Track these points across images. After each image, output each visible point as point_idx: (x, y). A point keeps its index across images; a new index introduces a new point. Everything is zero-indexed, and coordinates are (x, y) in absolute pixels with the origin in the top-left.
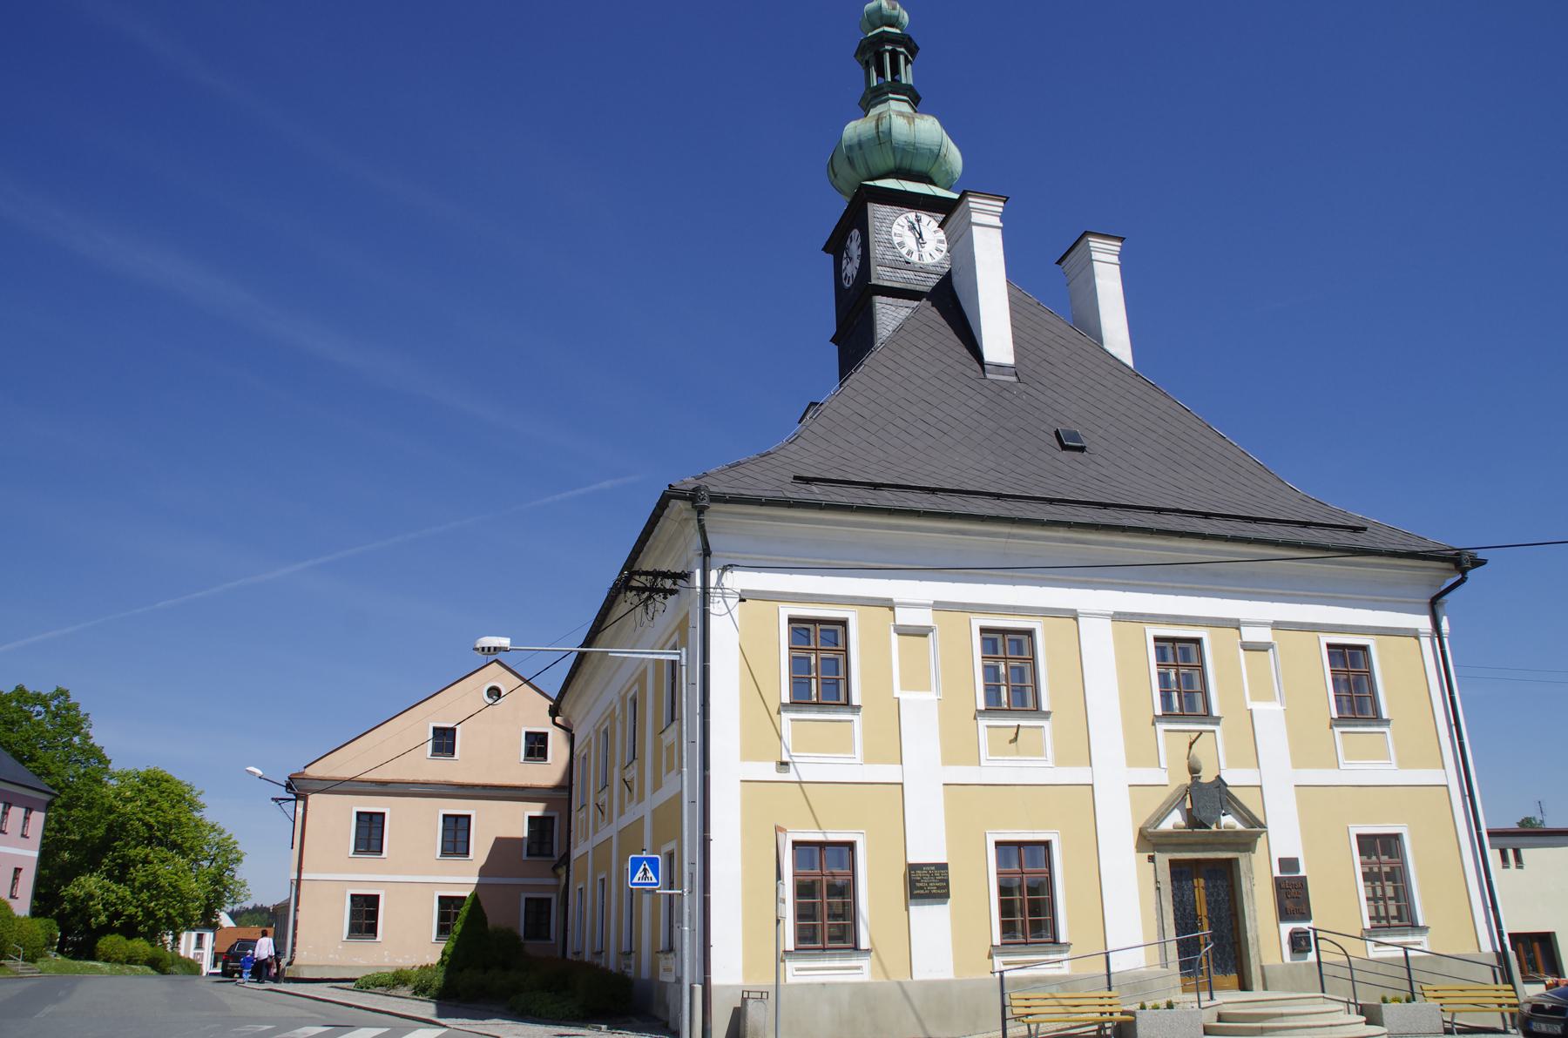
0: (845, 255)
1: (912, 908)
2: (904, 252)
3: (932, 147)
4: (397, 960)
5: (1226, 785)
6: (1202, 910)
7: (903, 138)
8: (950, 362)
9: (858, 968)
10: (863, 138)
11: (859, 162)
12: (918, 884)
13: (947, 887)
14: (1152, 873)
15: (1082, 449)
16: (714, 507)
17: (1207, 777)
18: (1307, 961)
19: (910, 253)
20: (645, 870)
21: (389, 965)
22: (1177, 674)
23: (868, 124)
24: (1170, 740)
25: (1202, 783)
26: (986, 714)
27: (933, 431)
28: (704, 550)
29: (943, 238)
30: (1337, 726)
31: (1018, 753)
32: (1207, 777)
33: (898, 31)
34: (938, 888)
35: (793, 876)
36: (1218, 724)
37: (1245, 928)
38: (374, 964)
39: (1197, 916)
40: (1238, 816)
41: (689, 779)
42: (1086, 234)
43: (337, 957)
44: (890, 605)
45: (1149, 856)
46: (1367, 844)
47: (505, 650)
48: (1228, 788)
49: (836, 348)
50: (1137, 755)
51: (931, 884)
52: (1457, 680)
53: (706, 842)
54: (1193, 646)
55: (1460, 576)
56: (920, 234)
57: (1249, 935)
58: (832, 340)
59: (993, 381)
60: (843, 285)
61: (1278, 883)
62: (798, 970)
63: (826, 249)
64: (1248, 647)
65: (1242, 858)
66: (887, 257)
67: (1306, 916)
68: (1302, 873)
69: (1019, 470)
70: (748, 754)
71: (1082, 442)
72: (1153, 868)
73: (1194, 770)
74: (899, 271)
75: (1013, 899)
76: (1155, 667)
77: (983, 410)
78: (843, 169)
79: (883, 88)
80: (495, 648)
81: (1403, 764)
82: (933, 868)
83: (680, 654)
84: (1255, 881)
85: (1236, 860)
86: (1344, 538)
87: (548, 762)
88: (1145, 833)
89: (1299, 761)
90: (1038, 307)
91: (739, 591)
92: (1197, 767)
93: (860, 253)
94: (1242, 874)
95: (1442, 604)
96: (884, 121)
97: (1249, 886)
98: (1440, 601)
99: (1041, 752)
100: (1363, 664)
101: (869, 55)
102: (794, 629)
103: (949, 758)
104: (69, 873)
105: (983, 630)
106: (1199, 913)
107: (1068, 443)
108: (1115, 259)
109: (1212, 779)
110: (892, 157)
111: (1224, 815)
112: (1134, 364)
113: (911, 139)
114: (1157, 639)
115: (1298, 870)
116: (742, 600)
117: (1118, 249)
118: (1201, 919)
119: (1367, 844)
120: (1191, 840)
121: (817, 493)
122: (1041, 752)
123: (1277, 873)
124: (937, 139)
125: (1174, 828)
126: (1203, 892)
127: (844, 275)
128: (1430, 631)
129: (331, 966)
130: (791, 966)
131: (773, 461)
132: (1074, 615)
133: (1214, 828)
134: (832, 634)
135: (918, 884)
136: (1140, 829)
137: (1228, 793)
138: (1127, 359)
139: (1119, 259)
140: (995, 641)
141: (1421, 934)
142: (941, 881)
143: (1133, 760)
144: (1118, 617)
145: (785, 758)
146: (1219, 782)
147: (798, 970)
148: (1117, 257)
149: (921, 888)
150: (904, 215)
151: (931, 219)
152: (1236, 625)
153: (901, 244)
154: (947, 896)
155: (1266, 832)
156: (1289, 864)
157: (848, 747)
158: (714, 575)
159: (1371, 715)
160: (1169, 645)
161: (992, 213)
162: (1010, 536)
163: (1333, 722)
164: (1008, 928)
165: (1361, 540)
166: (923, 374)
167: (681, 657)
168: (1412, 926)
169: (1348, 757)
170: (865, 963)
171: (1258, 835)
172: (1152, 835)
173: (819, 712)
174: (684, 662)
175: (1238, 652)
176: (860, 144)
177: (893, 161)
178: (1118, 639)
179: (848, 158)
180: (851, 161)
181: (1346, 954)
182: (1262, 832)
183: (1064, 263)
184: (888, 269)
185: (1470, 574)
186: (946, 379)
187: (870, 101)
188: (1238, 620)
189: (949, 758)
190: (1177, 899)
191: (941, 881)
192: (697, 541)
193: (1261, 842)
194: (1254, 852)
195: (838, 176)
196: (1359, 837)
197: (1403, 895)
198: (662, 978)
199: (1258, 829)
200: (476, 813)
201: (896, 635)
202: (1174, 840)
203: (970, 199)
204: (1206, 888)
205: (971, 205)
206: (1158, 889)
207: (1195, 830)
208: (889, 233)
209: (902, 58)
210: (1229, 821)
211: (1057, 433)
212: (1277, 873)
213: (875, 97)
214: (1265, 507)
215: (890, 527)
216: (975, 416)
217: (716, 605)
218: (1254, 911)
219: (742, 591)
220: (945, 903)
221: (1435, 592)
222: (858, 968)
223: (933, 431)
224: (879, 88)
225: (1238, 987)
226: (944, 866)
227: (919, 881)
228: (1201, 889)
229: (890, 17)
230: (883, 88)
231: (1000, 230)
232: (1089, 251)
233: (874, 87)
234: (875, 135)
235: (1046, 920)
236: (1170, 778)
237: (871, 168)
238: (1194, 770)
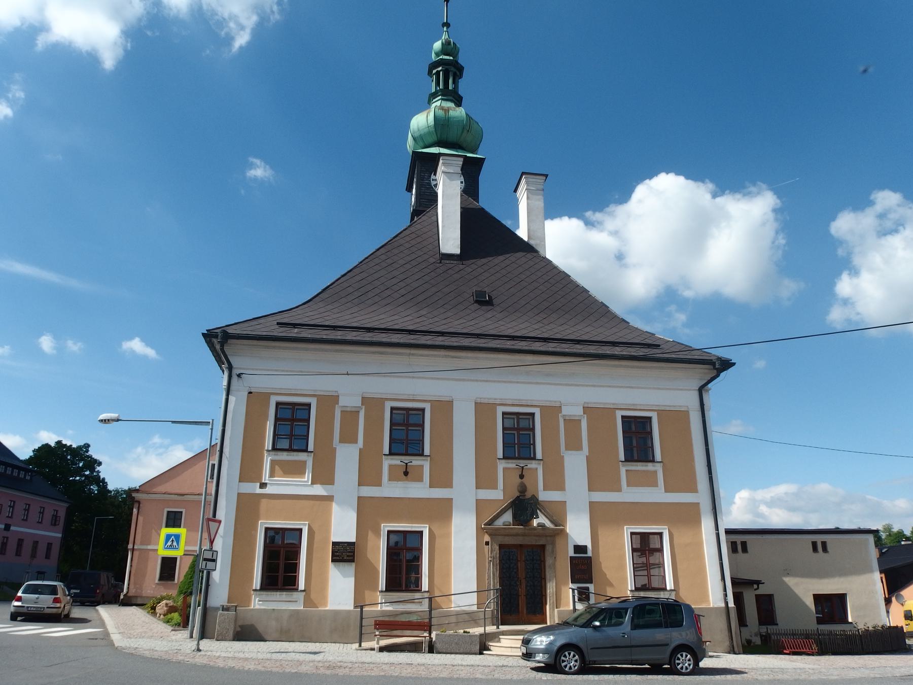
17: (528, 495)
18: (327, 608)
20: (173, 541)
31: (407, 480)
32: (528, 495)
33: (451, 58)
34: (348, 556)
45: (489, 542)
50: (483, 480)
51: (344, 554)
68: (590, 554)
75: (418, 565)
81: (667, 490)
82: (346, 545)
86: (641, 352)
95: (708, 391)
104: (881, 551)
115: (586, 553)
142: (350, 552)
146: (534, 498)
149: (338, 556)
191: (350, 552)
200: (186, 511)
225: (491, 624)
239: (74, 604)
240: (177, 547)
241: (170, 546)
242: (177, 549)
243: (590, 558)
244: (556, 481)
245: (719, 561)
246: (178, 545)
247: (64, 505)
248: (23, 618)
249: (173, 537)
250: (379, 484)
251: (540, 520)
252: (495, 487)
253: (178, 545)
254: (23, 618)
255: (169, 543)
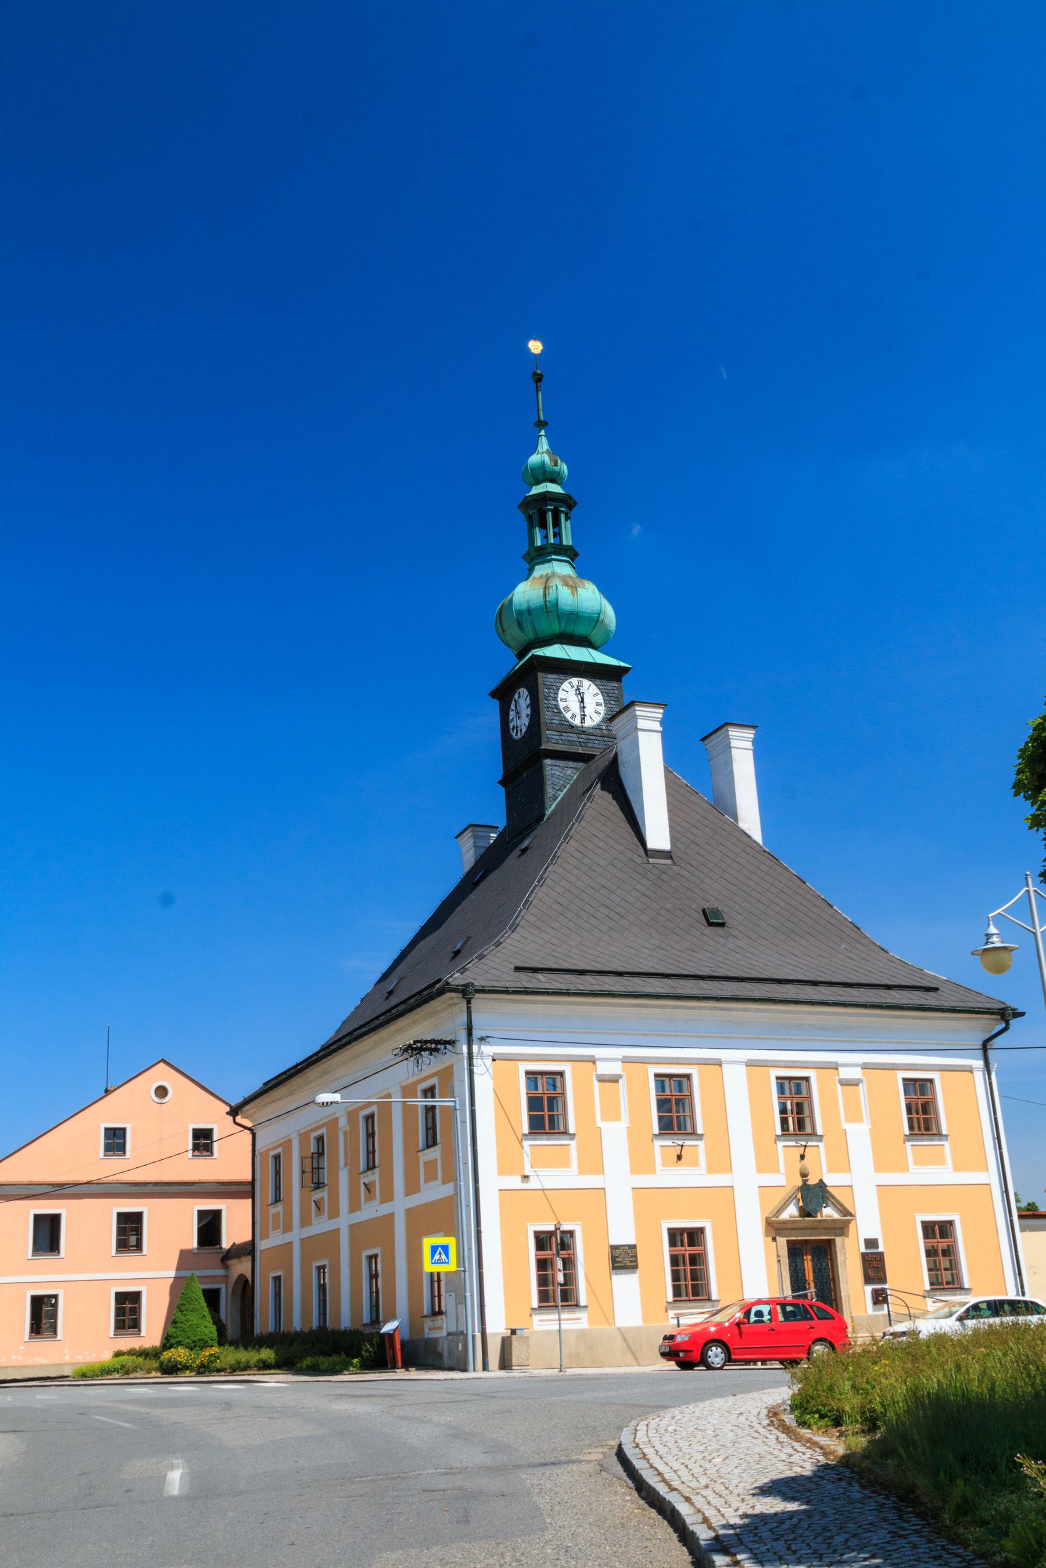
0: (513, 707)
1: (614, 1277)
2: (568, 716)
3: (593, 615)
4: (77, 1357)
5: (826, 1186)
6: (810, 1276)
7: (568, 608)
8: (621, 848)
9: (579, 1319)
10: (532, 606)
11: (528, 627)
12: (617, 1259)
13: (636, 1261)
14: (775, 1249)
15: (722, 925)
16: (477, 995)
19: (573, 716)
20: (440, 1253)
21: (70, 1362)
22: (791, 1103)
23: (536, 591)
24: (785, 1151)
25: (809, 1185)
26: (660, 1137)
27: (612, 915)
28: (468, 1026)
29: (602, 701)
30: (908, 1140)
31: (681, 1165)
32: (812, 1181)
34: (631, 1261)
35: (536, 1256)
36: (820, 1141)
37: (840, 1289)
38: (57, 1362)
39: (806, 1281)
40: (835, 1209)
41: (465, 1192)
42: (726, 724)
43: (20, 1358)
44: (593, 1061)
46: (930, 1229)
47: (337, 1103)
48: (828, 1188)
49: (503, 789)
50: (765, 1164)
52: (1001, 1100)
53: (479, 1233)
54: (804, 1083)
55: (1003, 1025)
56: (582, 699)
57: (842, 1294)
58: (500, 782)
59: (653, 864)
60: (511, 736)
61: (864, 1256)
62: (540, 1321)
63: (493, 694)
64: (845, 1083)
65: (838, 1241)
66: (554, 721)
67: (883, 1280)
68: (881, 1249)
69: (677, 946)
70: (503, 1171)
71: (723, 919)
72: (775, 1246)
73: (804, 1175)
74: (564, 734)
76: (777, 1098)
77: (648, 893)
78: (513, 631)
79: (546, 548)
80: (331, 1103)
81: (957, 1168)
82: (627, 1248)
83: (454, 1101)
84: (847, 1256)
85: (834, 1240)
87: (126, 1157)
88: (769, 1220)
89: (879, 1167)
90: (686, 788)
91: (492, 1054)
92: (806, 1173)
93: (529, 713)
94: (838, 1250)
96: (551, 591)
97: (842, 1259)
98: (990, 1043)
99: (696, 1164)
100: (930, 1094)
101: (533, 512)
102: (528, 1078)
103: (635, 1169)
105: (657, 1075)
106: (807, 1279)
107: (713, 919)
108: (749, 745)
109: (817, 1181)
110: (557, 623)
111: (825, 1207)
112: (763, 840)
113: (575, 609)
114: (778, 1078)
115: (877, 1247)
116: (494, 1060)
117: (752, 736)
118: (809, 1283)
119: (930, 1229)
120: (801, 1225)
121: (542, 981)
122: (696, 1164)
123: (863, 1249)
124: (596, 608)
125: (790, 1217)
126: (810, 1263)
127: (511, 725)
128: (982, 1067)
129: (14, 1367)
130: (536, 1318)
131: (504, 951)
132: (719, 1063)
133: (819, 1218)
134: (551, 1080)
135: (617, 1259)
136: (767, 1219)
137: (828, 1192)
138: (758, 836)
139: (753, 745)
140: (663, 1082)
141: (571, 1139)
142: (632, 1257)
143: (761, 1169)
144: (750, 1064)
145: (526, 1174)
146: (821, 1185)
147: (540, 1321)
148: (751, 743)
150: (569, 681)
151: (591, 683)
152: (835, 1067)
153: (567, 709)
154: (636, 1267)
155: (856, 1219)
156: (871, 1243)
157: (566, 1164)
158: (475, 1048)
159: (935, 1132)
160: (786, 1082)
161: (653, 719)
162: (675, 1007)
163: (906, 1138)
164: (677, 1291)
165: (930, 999)
166: (602, 862)
167: (456, 1103)
168: (961, 1288)
169: (916, 1163)
170: (583, 1315)
171: (849, 1221)
172: (774, 1222)
173: (548, 1139)
174: (458, 1107)
175: (836, 1086)
176: (529, 611)
177: (558, 628)
178: (750, 1080)
179: (518, 621)
180: (520, 625)
181: (907, 1306)
182: (853, 1220)
183: (707, 741)
184: (556, 733)
185: (1013, 1022)
186: (620, 865)
187: (534, 558)
188: (837, 1063)
189: (635, 1169)
190: (792, 1268)
191: (632, 1257)
192: (464, 1018)
193: (852, 1226)
194: (848, 1237)
195: (506, 632)
196: (923, 1222)
197: (954, 1267)
198: (428, 1334)
199: (849, 1218)
201: (597, 1082)
202: (790, 1226)
203: (637, 708)
204: (812, 1261)
205: (638, 713)
206: (779, 1261)
207: (806, 1218)
208: (555, 699)
209: (563, 516)
210: (828, 1212)
211: (704, 911)
212: (863, 1249)
213: (539, 555)
214: (859, 970)
215: (594, 1004)
216: (643, 899)
217: (479, 1068)
218: (846, 1276)
219: (494, 1054)
220: (635, 1273)
221: (988, 1036)
222: (579, 1319)
223: (612, 915)
224: (542, 548)
226: (634, 1247)
227: (617, 1257)
228: (809, 1261)
229: (553, 472)
230: (546, 548)
231: (660, 734)
232: (727, 738)
233: (537, 547)
234: (543, 603)
235: (702, 1284)
236: (787, 1181)
237: (538, 629)
238: (804, 1175)
239: (808, 1130)
240: (447, 1261)
241: (438, 1260)
242: (448, 1263)
243: (882, 1254)
244: (843, 1164)
245: (485, 1328)
246: (448, 1259)
247: (314, 1323)
248: (792, 1506)
249: (440, 1249)
250: (652, 1171)
251: (828, 1212)
252: (777, 1171)
253: (448, 1259)
254: (792, 1506)
255: (437, 1257)
